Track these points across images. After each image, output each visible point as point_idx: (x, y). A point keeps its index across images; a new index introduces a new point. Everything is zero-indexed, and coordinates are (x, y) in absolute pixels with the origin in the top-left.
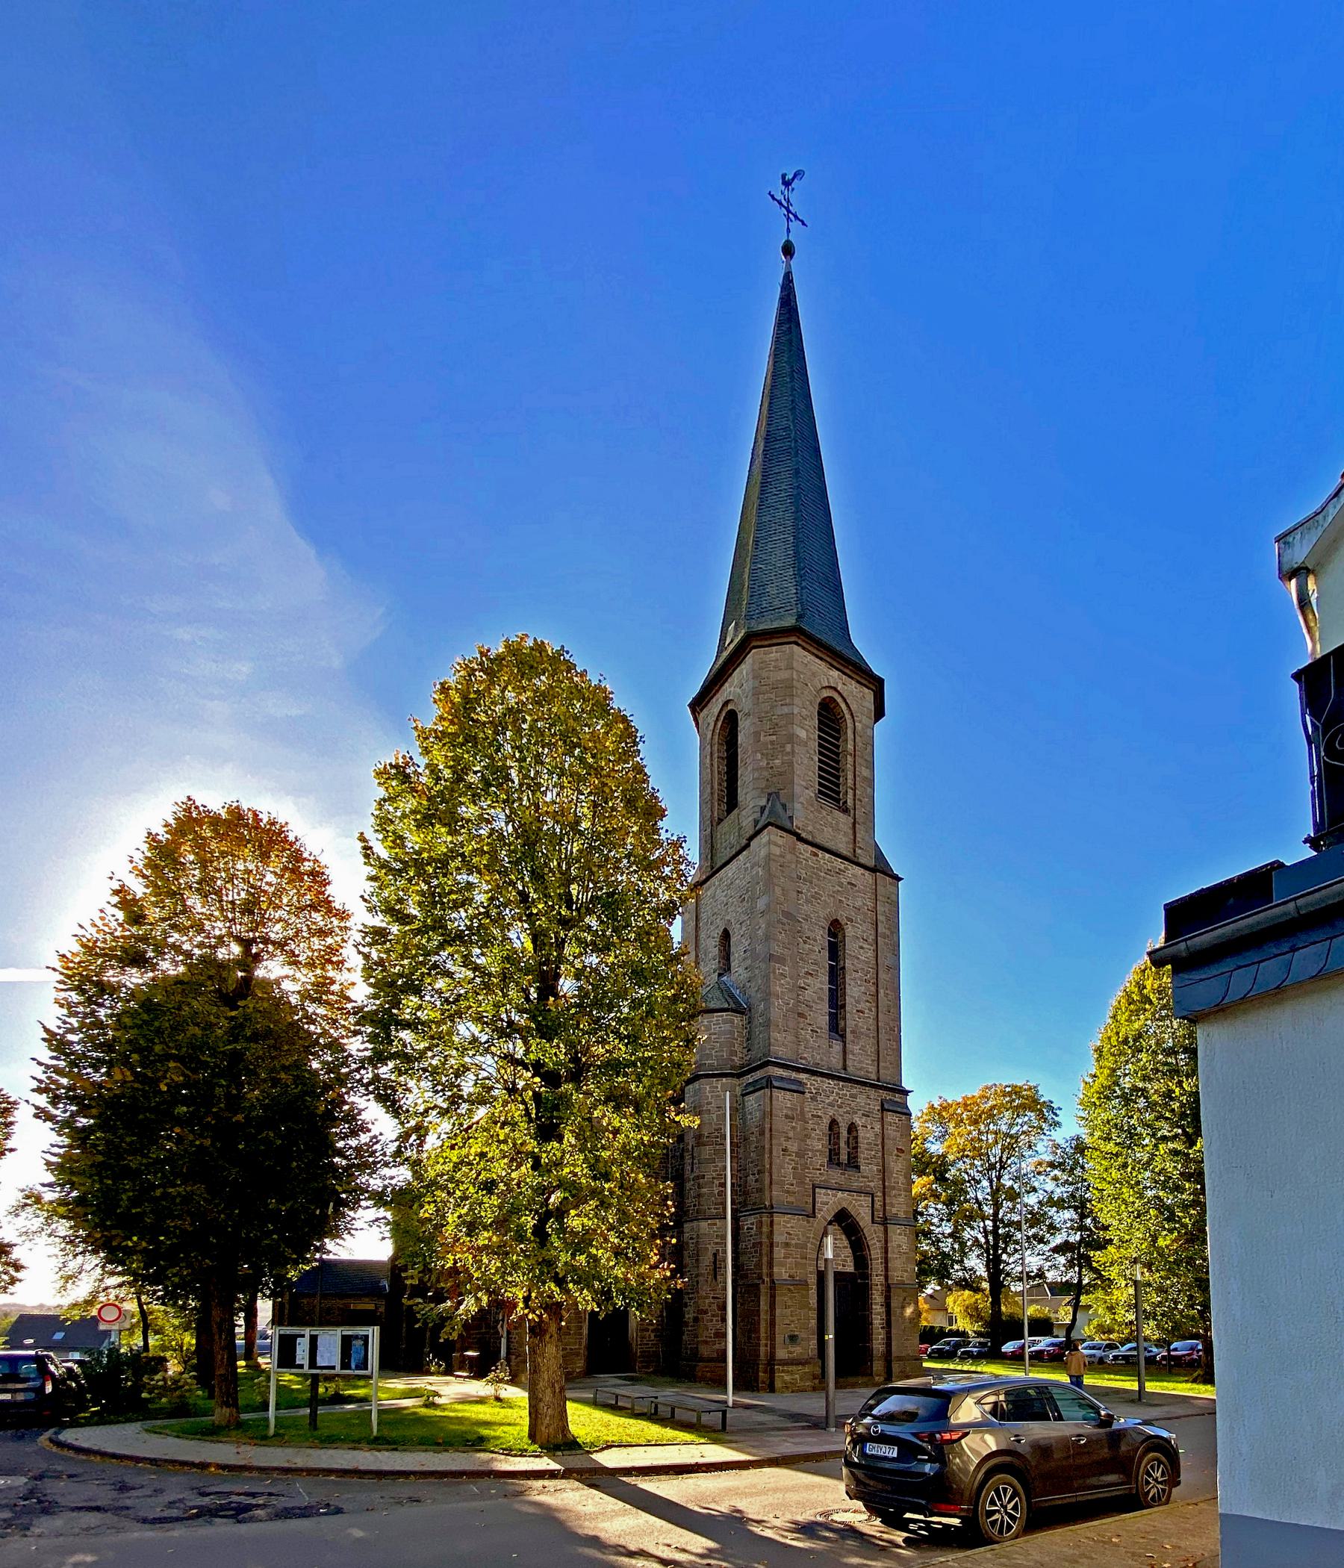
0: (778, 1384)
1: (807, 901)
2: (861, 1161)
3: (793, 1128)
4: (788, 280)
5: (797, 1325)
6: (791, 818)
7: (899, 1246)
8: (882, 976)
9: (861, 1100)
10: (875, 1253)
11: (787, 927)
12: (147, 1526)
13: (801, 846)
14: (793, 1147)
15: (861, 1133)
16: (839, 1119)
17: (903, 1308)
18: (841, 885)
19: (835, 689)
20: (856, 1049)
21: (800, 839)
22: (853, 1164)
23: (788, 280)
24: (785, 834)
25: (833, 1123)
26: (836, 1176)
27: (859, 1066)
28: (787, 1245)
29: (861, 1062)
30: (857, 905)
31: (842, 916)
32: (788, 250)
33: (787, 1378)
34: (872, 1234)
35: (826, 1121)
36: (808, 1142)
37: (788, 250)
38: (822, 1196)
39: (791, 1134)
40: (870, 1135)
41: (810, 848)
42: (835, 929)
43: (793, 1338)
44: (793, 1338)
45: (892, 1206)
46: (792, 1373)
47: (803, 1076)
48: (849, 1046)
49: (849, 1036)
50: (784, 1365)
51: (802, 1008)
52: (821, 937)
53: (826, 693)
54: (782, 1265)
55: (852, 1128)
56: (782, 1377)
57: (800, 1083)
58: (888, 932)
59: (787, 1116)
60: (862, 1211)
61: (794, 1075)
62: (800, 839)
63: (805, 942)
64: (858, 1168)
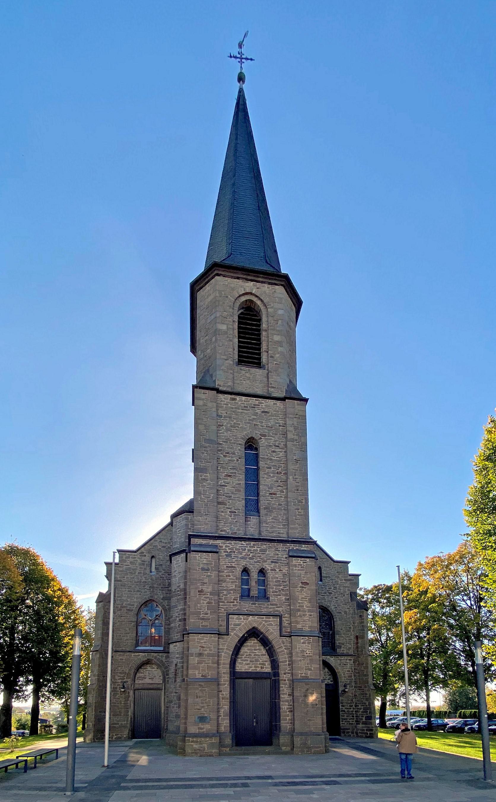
0: (188, 750)
1: (227, 430)
2: (270, 592)
3: (208, 576)
4: (241, 91)
5: (207, 710)
6: (215, 381)
7: (303, 651)
8: (291, 467)
9: (270, 553)
10: (283, 658)
11: (208, 449)
12: (203, 759)
13: (221, 396)
14: (208, 589)
15: (270, 574)
16: (251, 567)
17: (306, 696)
18: (256, 414)
19: (251, 294)
20: (269, 519)
21: (218, 391)
22: (264, 596)
23: (241, 91)
24: (207, 391)
25: (245, 571)
26: (247, 606)
27: (271, 530)
28: (200, 655)
29: (272, 525)
30: (270, 425)
31: (256, 435)
32: (241, 78)
33: (196, 746)
34: (280, 645)
35: (239, 570)
36: (224, 584)
37: (241, 78)
38: (234, 620)
39: (206, 580)
40: (279, 576)
41: (230, 396)
42: (251, 445)
43: (202, 719)
44: (202, 719)
45: (297, 623)
46: (201, 743)
47: (219, 542)
48: (263, 518)
49: (262, 512)
50: (193, 737)
51: (222, 499)
52: (240, 450)
53: (243, 299)
54: (195, 668)
55: (262, 572)
56: (192, 745)
57: (216, 546)
58: (296, 437)
59: (203, 569)
60: (270, 627)
61: (211, 542)
62: (218, 391)
63: (225, 456)
64: (268, 599)
